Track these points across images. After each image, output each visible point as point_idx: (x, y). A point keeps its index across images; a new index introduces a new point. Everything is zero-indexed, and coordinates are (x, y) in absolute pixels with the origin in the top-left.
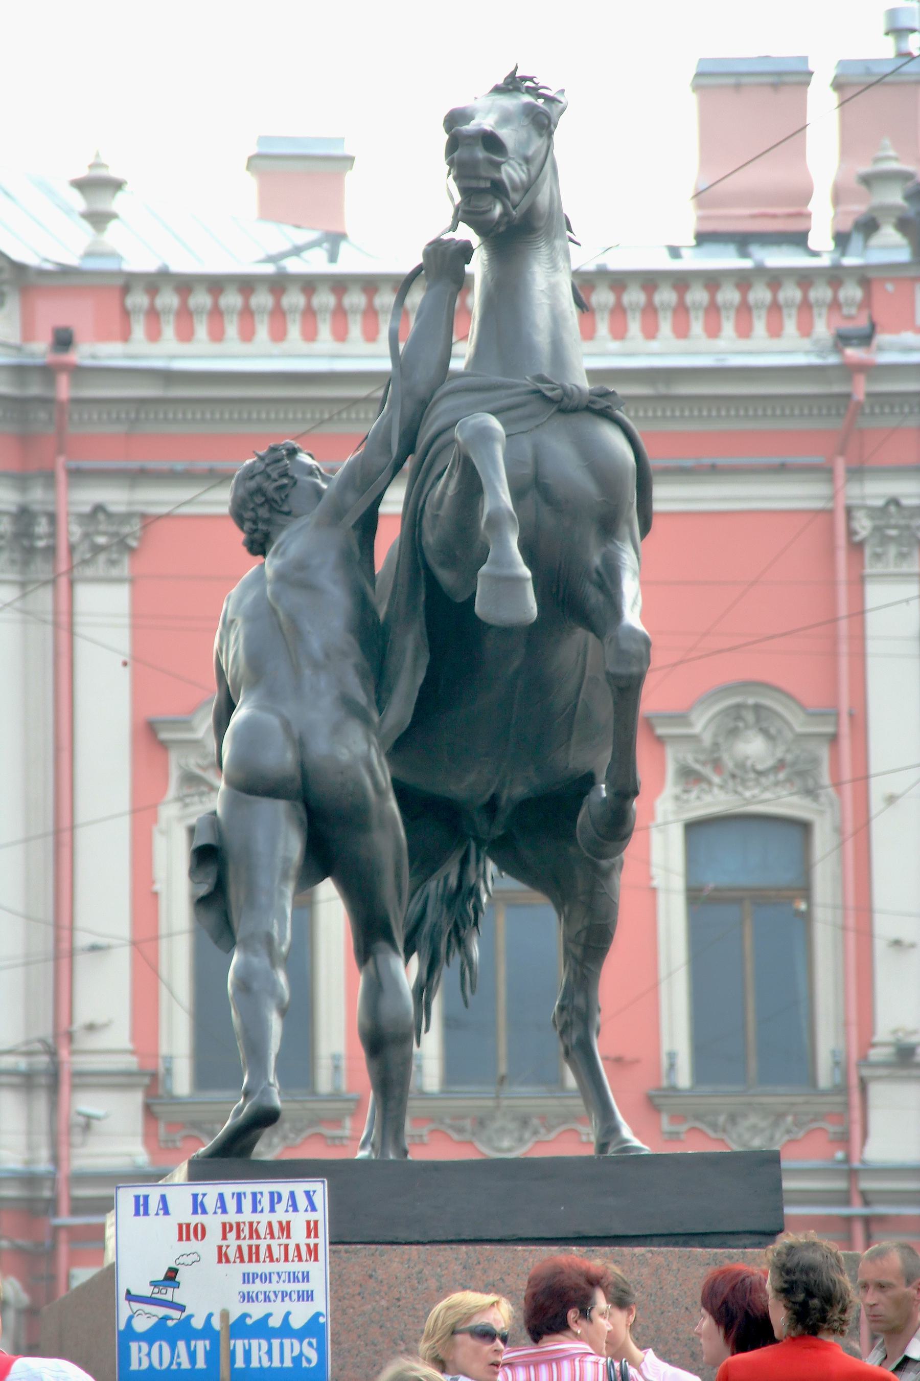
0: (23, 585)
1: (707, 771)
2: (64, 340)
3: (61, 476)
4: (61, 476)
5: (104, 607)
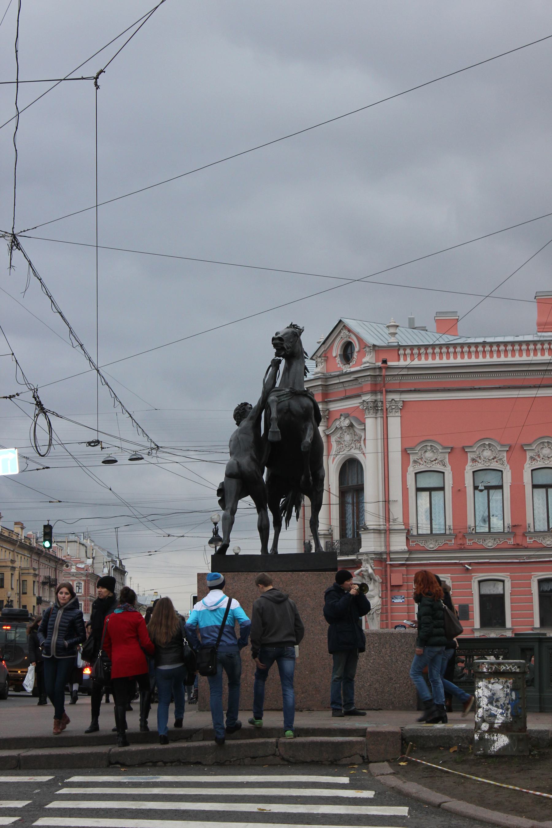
0: (376, 418)
1: (537, 457)
2: (385, 362)
3: (384, 392)
4: (384, 392)
5: (395, 423)
